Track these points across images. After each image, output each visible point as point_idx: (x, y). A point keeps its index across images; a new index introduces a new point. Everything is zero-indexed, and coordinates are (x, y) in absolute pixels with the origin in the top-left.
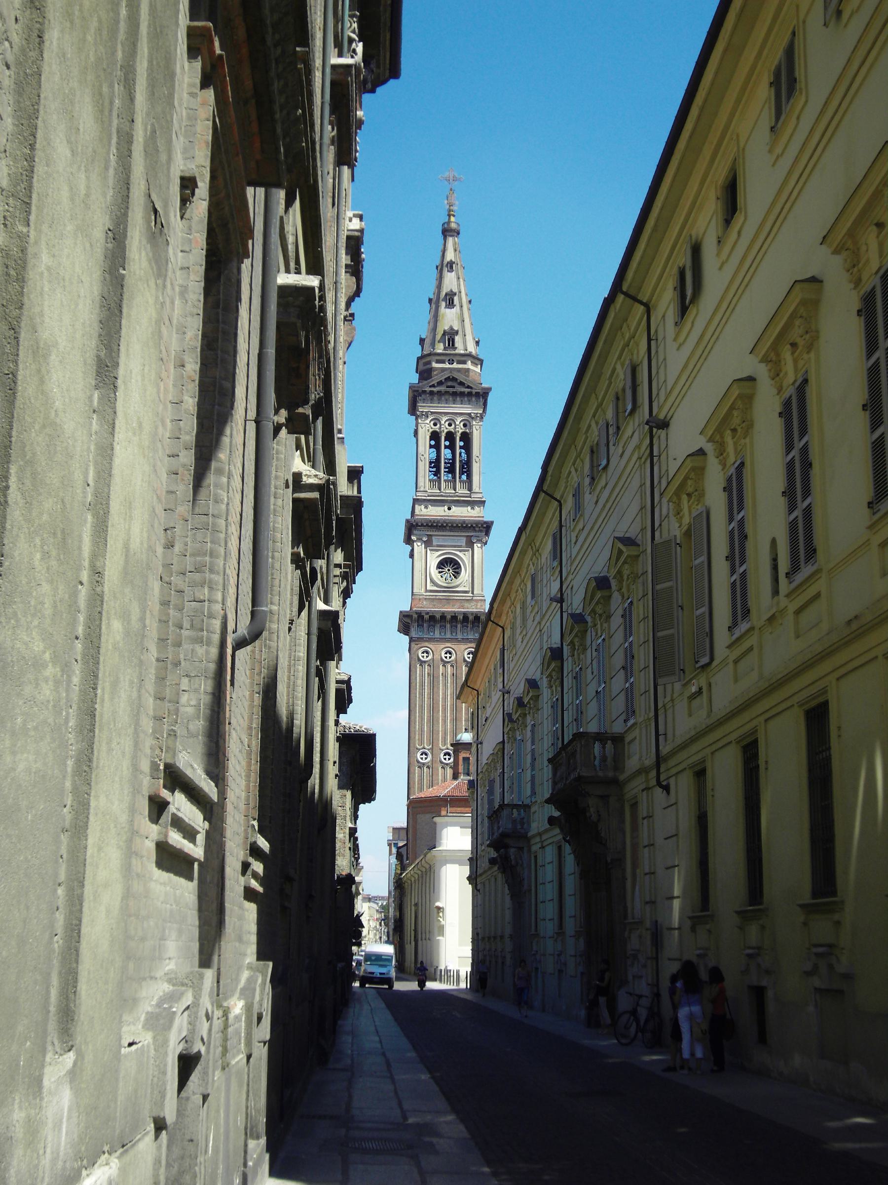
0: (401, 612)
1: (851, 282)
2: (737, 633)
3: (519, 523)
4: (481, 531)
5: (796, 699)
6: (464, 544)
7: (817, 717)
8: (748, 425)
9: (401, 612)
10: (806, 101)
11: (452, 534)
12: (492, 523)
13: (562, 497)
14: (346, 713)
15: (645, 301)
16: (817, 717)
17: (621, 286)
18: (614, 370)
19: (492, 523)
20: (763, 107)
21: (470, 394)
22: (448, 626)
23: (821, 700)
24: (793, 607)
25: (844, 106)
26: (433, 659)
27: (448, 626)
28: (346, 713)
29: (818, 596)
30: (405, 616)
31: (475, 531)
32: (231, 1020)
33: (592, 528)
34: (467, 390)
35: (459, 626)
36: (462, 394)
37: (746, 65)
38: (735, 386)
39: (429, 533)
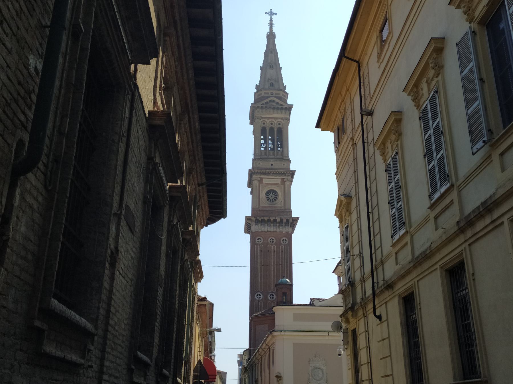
0: (246, 217)
1: (467, 21)
2: (397, 237)
3: (333, 67)
5: (437, 266)
6: (280, 183)
7: (456, 275)
8: (439, 68)
10: (392, 36)
15: (357, 60)
16: (456, 275)
17: (344, 54)
18: (337, 115)
20: (374, 46)
21: (282, 109)
23: (410, 291)
24: (433, 215)
25: (384, 83)
29: (452, 202)
33: (345, 153)
34: (280, 107)
35: (278, 225)
38: (393, 114)
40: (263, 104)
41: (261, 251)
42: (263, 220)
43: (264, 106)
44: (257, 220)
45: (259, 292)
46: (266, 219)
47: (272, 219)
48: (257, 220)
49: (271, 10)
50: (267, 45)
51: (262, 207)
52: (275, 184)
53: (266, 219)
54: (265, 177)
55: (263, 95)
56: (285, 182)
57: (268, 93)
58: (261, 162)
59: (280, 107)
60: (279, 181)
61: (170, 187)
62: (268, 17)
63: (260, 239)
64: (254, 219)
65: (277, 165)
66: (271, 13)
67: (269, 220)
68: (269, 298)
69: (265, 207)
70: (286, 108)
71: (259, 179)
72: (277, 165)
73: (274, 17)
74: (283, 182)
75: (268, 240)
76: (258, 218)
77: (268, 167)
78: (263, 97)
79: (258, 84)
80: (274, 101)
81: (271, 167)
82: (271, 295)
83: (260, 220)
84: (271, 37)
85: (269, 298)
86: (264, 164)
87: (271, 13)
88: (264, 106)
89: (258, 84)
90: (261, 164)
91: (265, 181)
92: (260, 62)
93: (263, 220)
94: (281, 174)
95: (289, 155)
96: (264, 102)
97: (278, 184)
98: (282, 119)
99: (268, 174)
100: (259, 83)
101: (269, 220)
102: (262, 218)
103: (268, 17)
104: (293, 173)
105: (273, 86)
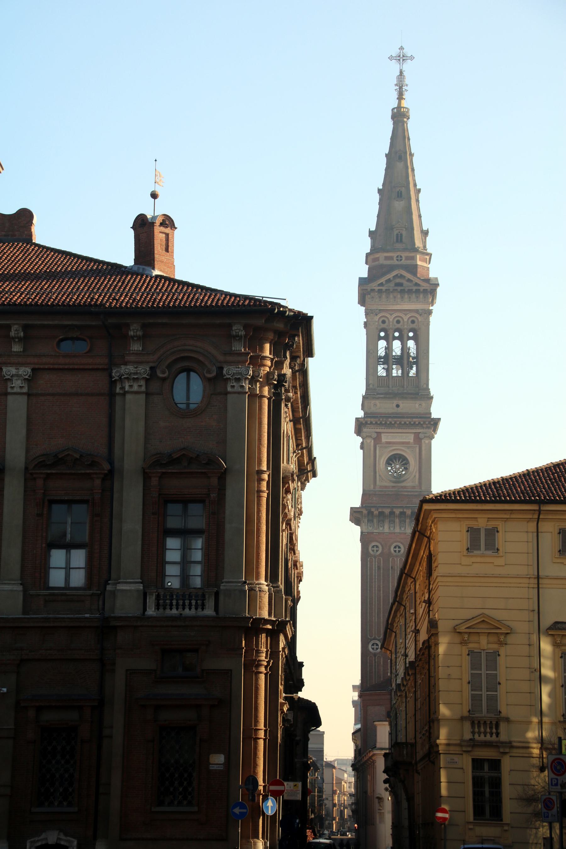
0: (351, 508)
4: (429, 428)
6: (412, 441)
9: (351, 508)
11: (400, 431)
12: (439, 419)
13: (415, 577)
14: (301, 691)
19: (439, 419)
21: (418, 291)
22: (397, 520)
26: (382, 553)
27: (397, 520)
28: (301, 691)
30: (355, 512)
31: (423, 428)
32: (428, 724)
34: (414, 288)
36: (410, 291)
37: (300, 819)
39: (378, 430)
40: (381, 284)
41: (379, 568)
42: (381, 514)
43: (384, 288)
44: (370, 513)
45: (375, 639)
46: (387, 511)
47: (397, 511)
48: (370, 513)
49: (402, 48)
50: (386, 170)
51: (381, 487)
52: (403, 443)
53: (387, 511)
54: (385, 430)
55: (382, 261)
56: (421, 439)
57: (391, 258)
58: (377, 402)
59: (414, 288)
60: (410, 438)
61: (274, 617)
62: (395, 68)
63: (377, 547)
64: (365, 512)
65: (408, 406)
66: (401, 58)
67: (392, 513)
68: (371, 650)
69: (386, 487)
70: (425, 291)
71: (375, 435)
72: (408, 406)
73: (407, 67)
74: (418, 439)
75: (390, 549)
76: (373, 510)
77: (391, 411)
78: (382, 266)
79: (381, 187)
80: (402, 276)
81: (396, 410)
82: (373, 645)
83: (376, 513)
84: (399, 117)
85: (371, 650)
86: (386, 407)
87: (401, 58)
88: (384, 288)
89: (381, 187)
90: (378, 405)
91: (384, 439)
92: (378, 179)
93: (381, 514)
94: (414, 425)
95: (430, 386)
96: (383, 280)
97: (408, 443)
98: (417, 311)
99: (391, 426)
100: (383, 185)
101: (392, 513)
102: (380, 510)
103: (395, 68)
104: (436, 422)
105: (401, 241)
